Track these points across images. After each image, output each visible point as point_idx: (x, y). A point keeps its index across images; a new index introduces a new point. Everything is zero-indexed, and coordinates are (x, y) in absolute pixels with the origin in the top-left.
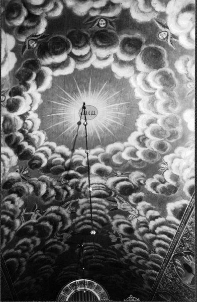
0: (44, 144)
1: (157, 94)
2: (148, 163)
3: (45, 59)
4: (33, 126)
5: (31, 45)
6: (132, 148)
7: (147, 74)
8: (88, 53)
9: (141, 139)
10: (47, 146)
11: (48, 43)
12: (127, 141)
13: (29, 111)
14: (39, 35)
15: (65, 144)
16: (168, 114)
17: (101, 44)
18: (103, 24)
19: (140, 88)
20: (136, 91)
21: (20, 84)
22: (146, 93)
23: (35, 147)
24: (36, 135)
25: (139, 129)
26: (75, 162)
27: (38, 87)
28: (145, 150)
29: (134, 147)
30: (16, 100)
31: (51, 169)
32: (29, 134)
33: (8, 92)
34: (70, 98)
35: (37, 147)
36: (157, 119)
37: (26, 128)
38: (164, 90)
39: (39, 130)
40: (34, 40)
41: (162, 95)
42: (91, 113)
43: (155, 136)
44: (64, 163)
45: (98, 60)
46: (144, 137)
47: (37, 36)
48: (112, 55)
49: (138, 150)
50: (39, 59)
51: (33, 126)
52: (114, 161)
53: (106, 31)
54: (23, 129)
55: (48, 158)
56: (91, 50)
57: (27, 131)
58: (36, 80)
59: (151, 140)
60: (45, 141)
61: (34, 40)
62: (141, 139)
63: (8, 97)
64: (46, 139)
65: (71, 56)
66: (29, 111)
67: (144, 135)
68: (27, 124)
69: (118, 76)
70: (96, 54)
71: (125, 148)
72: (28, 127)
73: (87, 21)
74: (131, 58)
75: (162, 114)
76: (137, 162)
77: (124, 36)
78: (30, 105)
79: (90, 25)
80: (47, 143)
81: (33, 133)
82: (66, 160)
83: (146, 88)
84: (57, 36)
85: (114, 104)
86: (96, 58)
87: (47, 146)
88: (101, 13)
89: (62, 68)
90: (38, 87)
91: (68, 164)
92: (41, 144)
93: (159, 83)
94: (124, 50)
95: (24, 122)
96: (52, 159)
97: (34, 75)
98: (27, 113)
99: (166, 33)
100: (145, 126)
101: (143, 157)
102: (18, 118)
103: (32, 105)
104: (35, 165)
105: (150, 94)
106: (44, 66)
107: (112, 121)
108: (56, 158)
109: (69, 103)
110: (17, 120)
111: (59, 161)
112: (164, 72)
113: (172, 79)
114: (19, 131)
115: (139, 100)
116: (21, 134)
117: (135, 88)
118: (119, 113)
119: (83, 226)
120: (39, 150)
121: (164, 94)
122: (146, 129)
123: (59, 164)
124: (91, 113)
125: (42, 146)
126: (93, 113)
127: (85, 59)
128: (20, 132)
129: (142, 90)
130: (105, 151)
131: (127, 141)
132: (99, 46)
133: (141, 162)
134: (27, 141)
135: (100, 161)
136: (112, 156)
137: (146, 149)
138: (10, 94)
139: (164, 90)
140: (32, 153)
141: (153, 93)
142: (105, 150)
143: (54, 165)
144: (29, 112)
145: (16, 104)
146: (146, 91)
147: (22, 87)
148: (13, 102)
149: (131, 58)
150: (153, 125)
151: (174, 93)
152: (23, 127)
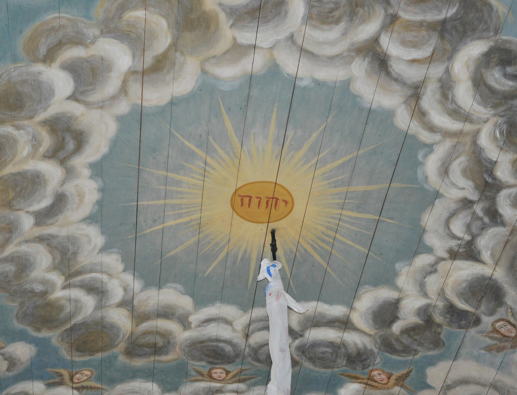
0: (437, 137)
1: (57, 279)
2: (15, 59)
3: (360, 345)
4: (453, 215)
5: (383, 376)
6: (95, 97)
7: (100, 306)
8: (253, 332)
9: (71, 145)
10: (432, 129)
11: (346, 366)
12: (120, 119)
13: (444, 259)
14: (360, 383)
15: (361, 109)
16: (10, 250)
17: (221, 345)
18: (218, 372)
19: (110, 275)
20: (120, 267)
21: (439, 326)
22: (91, 271)
23: (474, 143)
24: (454, 185)
25: (86, 172)
26: (337, 22)
27: (398, 301)
28: (45, 109)
29: (87, 104)
30: (467, 301)
31: (452, 12)
32: (473, 196)
33: (480, 328)
34: (314, 249)
35: (468, 140)
36: (37, 224)
37: (475, 217)
38: (44, 294)
39: (437, 195)
40: (375, 381)
41: (44, 282)
42: (255, 201)
43: (23, 175)
44: (384, 27)
45: (230, 318)
46: (61, 154)
47: (366, 384)
48: (193, 326)
49: (73, 97)
50: (376, 350)
51: (453, 215)
52: (164, 23)
53: (210, 363)
54: (486, 220)
55: (447, 71)
56: (247, 336)
57: (478, 209)
58: (395, 318)
59: (32, 155)
60: (430, 148)
61: (375, 381)
62: (71, 145)
63: (487, 320)
64: (425, 156)
65: (297, 333)
66: (444, 259)
67: (62, 162)
68: (468, 227)
69: (175, 289)
70: (234, 330)
71: (124, 90)
72: (469, 219)
73: (252, 378)
74: (145, 326)
75: (27, 241)
76: (60, 45)
77: (170, 357)
78: (435, 271)
79: (245, 372)
80: (425, 136)
81: (460, 194)
82: (376, 40)
83: (94, 279)
84: (322, 370)
85: (178, 225)
86: (234, 324)
87: (432, 129)
88: (223, 387)
89: (322, 315)
90: (398, 301)
91: (364, 20)
92: (448, 144)
93: (62, 302)
94: (166, 335)
95: (474, 237)
96: (430, 60)
97: (397, 328)
98: (453, 255)
99: (76, 381)
100: (70, 188)
101: (44, 77)
102: (486, 256)
103: (429, 269)
104: (509, 70)
105: (79, 273)
106: (370, 335)
107: (185, 179)
108: (414, 61)
109: (319, 238)
110: (492, 255)
111: (404, 43)
112: (56, 327)
113: (31, 324)
114: (503, 224)
115: (104, 249)
116: (501, 211)
117: (124, 271)
118: (161, 202)
119: (321, 39)
120: (468, 127)
121: (39, 288)
122: (63, 182)
123: (409, 26)
124: (255, 201)
125: (447, 134)
126: (246, 200)
127: (262, 323)
128: (501, 216)
129: (102, 272)
130: (202, 63)
131: (120, 119)
132: (228, 342)
133: (43, 50)
134: (494, 178)
135: (222, 16)
136: (174, 46)
137: (42, 116)
138: (477, 321)
139: (44, 294)
140: (495, 125)
141: (69, 277)
142: (204, 72)
143: (431, 26)
144: (446, 255)
145: (474, 294)
146: (93, 275)
147: (438, 318)
148: (480, 301)
149: (145, 326)
150: (45, 203)
151: (13, 301)
152: (484, 228)
